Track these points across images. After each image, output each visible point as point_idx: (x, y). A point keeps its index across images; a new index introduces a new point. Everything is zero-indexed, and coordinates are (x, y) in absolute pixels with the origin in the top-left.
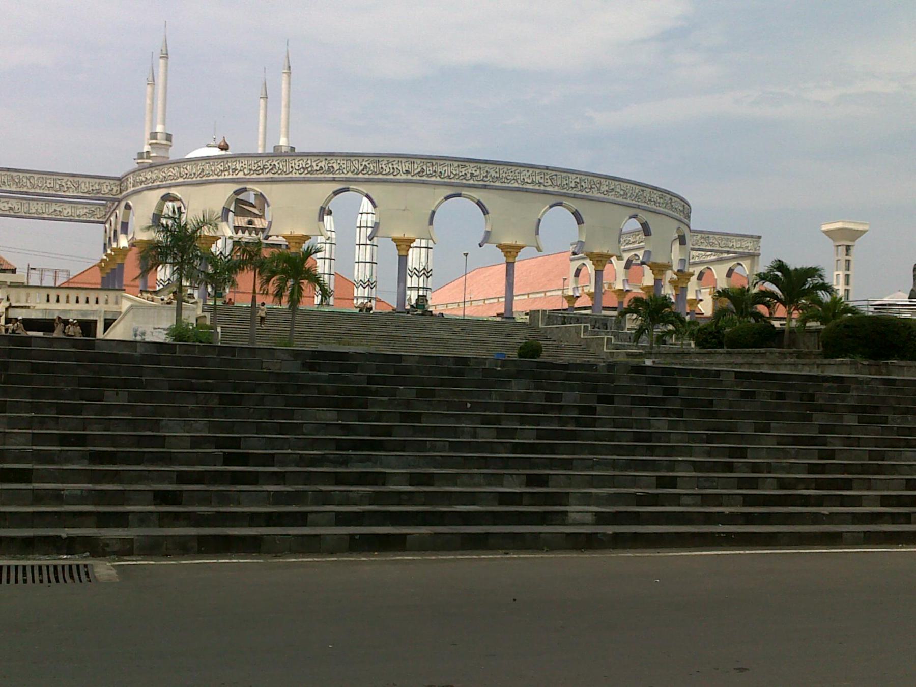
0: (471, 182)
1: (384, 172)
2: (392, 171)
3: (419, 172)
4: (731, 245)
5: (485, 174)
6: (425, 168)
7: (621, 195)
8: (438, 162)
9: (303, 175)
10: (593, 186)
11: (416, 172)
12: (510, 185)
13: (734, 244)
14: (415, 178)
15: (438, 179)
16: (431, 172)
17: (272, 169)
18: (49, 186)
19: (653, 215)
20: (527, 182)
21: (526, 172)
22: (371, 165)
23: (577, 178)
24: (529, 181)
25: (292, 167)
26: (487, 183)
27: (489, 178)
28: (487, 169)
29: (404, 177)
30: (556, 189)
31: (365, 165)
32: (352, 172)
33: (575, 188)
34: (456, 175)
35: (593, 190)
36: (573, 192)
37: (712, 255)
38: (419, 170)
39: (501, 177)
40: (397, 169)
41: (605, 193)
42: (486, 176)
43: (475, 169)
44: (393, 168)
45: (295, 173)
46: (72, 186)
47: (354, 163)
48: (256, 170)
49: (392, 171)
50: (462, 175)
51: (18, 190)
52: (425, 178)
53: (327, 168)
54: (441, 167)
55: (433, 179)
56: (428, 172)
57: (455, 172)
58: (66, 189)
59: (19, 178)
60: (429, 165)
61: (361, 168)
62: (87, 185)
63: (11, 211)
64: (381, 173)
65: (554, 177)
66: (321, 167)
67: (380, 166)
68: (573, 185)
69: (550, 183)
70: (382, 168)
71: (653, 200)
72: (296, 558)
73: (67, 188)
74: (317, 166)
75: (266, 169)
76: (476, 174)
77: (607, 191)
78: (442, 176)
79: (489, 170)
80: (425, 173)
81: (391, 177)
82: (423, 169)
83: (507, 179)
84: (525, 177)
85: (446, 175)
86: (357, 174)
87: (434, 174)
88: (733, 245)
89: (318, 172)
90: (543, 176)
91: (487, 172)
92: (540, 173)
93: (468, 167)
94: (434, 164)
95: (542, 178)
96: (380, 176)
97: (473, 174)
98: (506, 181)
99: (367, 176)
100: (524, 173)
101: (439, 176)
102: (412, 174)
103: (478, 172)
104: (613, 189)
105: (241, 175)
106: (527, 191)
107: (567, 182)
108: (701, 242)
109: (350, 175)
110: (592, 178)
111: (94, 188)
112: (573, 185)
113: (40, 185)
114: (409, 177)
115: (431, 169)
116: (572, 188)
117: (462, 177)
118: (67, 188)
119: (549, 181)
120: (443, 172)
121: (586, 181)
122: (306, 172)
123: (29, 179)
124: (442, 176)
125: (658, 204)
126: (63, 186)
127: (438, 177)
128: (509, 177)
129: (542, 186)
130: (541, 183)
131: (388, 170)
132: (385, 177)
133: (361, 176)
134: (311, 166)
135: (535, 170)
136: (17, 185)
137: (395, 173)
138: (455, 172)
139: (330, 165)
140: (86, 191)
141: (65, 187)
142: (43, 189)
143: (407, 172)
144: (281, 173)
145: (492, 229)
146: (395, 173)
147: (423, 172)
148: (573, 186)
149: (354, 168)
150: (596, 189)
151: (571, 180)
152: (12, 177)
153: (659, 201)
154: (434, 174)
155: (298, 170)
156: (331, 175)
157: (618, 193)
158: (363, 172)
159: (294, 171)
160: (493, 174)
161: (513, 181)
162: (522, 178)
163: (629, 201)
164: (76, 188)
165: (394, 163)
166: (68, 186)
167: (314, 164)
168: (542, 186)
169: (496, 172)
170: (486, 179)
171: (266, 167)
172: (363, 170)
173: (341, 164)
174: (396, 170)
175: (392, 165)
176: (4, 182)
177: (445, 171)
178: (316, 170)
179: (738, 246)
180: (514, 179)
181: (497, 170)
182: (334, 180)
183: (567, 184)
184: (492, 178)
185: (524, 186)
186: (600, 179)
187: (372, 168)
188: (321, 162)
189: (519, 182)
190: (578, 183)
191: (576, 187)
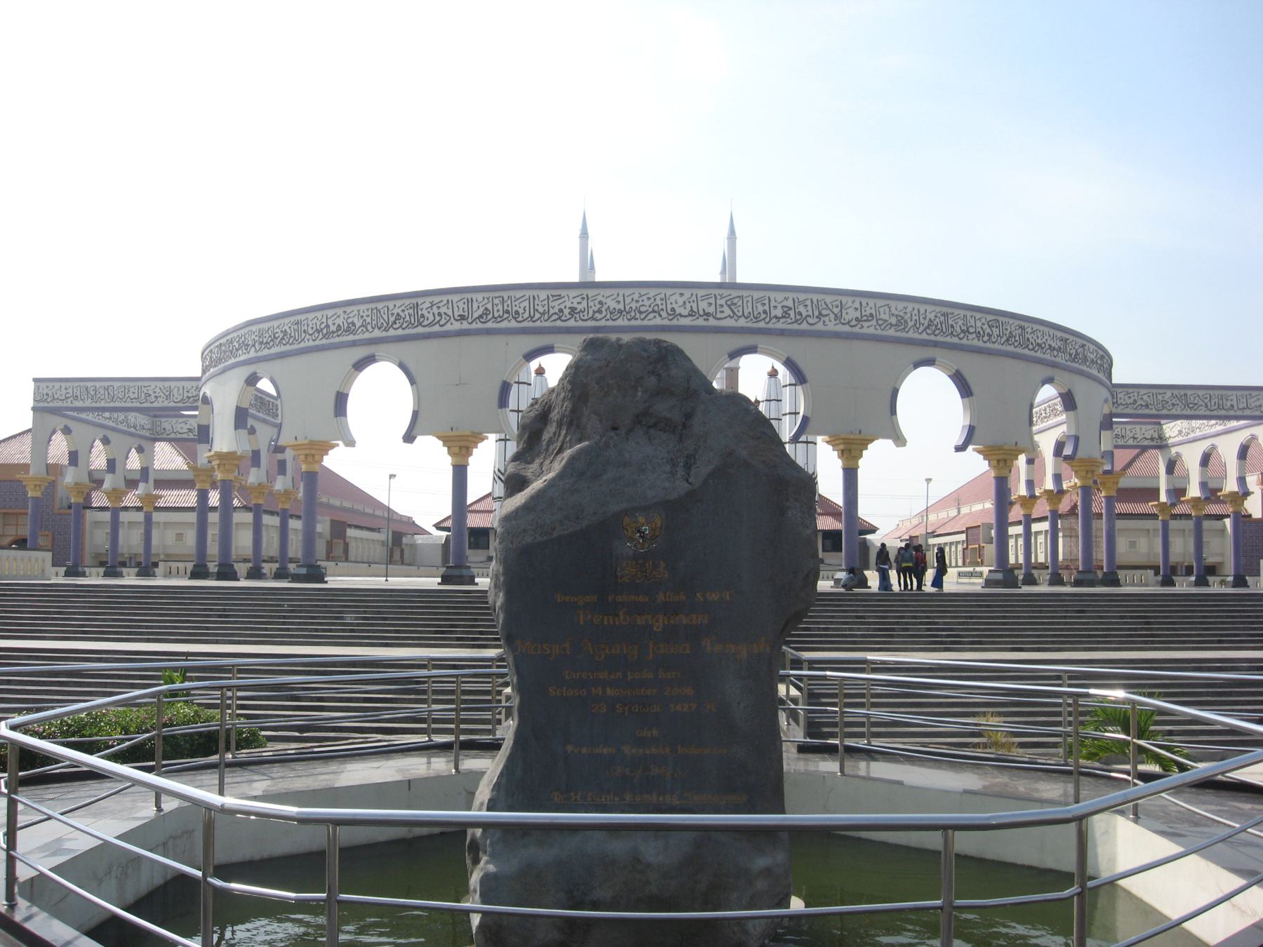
0: (571, 323)
1: (426, 323)
2: (438, 318)
3: (481, 316)
4: (1229, 405)
5: (599, 306)
6: (490, 308)
7: (891, 325)
8: (512, 293)
9: (317, 342)
10: (824, 312)
11: (476, 315)
12: (646, 323)
13: (1234, 403)
14: (474, 326)
15: (513, 324)
16: (501, 313)
17: (283, 339)
18: (132, 397)
19: (975, 358)
20: (681, 315)
21: (677, 297)
22: (406, 312)
23: (786, 299)
24: (685, 312)
25: (304, 331)
26: (603, 323)
27: (604, 313)
28: (600, 298)
29: (457, 326)
30: (742, 322)
31: (398, 314)
32: (379, 328)
33: (783, 317)
34: (543, 314)
35: (826, 319)
36: (780, 325)
37: (1217, 423)
38: (482, 309)
39: (627, 309)
40: (445, 313)
41: (854, 323)
42: (599, 311)
43: (579, 299)
44: (440, 314)
45: (308, 340)
46: (162, 394)
47: (382, 311)
48: (267, 343)
49: (438, 318)
50: (556, 313)
51: (94, 405)
52: (490, 325)
53: (346, 325)
54: (517, 303)
55: (504, 325)
56: (496, 315)
57: (541, 310)
58: (154, 400)
59: (95, 390)
60: (496, 301)
61: (392, 319)
62: (181, 391)
63: (190, 434)
64: (420, 324)
65: (735, 301)
66: (339, 325)
67: (420, 312)
68: (779, 312)
69: (728, 312)
70: (423, 316)
71: (971, 330)
72: (502, 624)
73: (156, 397)
74: (334, 324)
75: (277, 338)
76: (579, 307)
77: (857, 319)
78: (520, 319)
79: (604, 300)
80: (491, 316)
81: (436, 328)
82: (486, 309)
83: (641, 313)
84: (675, 306)
85: (526, 315)
86: (386, 330)
87: (506, 316)
88: (1232, 406)
89: (335, 335)
90: (712, 301)
91: (601, 303)
92: (707, 296)
93: (566, 298)
94: (506, 299)
95: (710, 304)
96: (420, 330)
97: (576, 309)
98: (638, 316)
99: (400, 332)
100: (673, 299)
101: (515, 318)
102: (470, 320)
103: (584, 304)
104: (871, 315)
105: (252, 354)
106: (990, 352)
107: (767, 308)
108: (1173, 405)
109: (377, 333)
110: (820, 297)
111: (190, 395)
112: (779, 312)
113: (121, 397)
114: (465, 325)
115: (500, 307)
116: (776, 317)
117: (555, 317)
118: (156, 397)
119: (726, 309)
120: (521, 311)
121: (808, 303)
122: (321, 336)
123: (107, 390)
124: (520, 319)
125: (986, 338)
126: (150, 395)
127: (513, 321)
128: (643, 309)
129: (711, 319)
130: (708, 314)
131: (431, 318)
132: (427, 330)
133: (392, 332)
134: (327, 326)
135: (695, 291)
136: (92, 399)
137: (441, 323)
138: (541, 310)
139: (350, 321)
140: (179, 400)
141: (153, 396)
142: (125, 402)
143: (462, 318)
144: (292, 344)
145: (892, 419)
146: (441, 323)
147: (487, 315)
148: (894, 323)
149: (382, 321)
150: (832, 316)
151: (773, 304)
152: (87, 388)
153: (988, 330)
154: (506, 316)
155: (311, 335)
156: (351, 337)
157: (885, 321)
158: (395, 326)
159: (308, 337)
160: (613, 305)
161: (651, 316)
162: (669, 307)
163: (911, 335)
164: (167, 396)
165: (440, 305)
166: (157, 394)
167: (330, 322)
168: (711, 319)
169: (619, 302)
170: (598, 316)
171: (277, 335)
172: (395, 323)
173: (365, 317)
174: (444, 316)
175: (439, 307)
176: (77, 396)
177: (524, 310)
178: (333, 332)
179: (1241, 406)
180: (654, 311)
181: (621, 298)
182: (354, 344)
183: (765, 312)
184: (611, 313)
185: (675, 322)
186: (840, 298)
187: (407, 318)
188: (339, 317)
189: (664, 314)
190: (790, 309)
191: (786, 315)
